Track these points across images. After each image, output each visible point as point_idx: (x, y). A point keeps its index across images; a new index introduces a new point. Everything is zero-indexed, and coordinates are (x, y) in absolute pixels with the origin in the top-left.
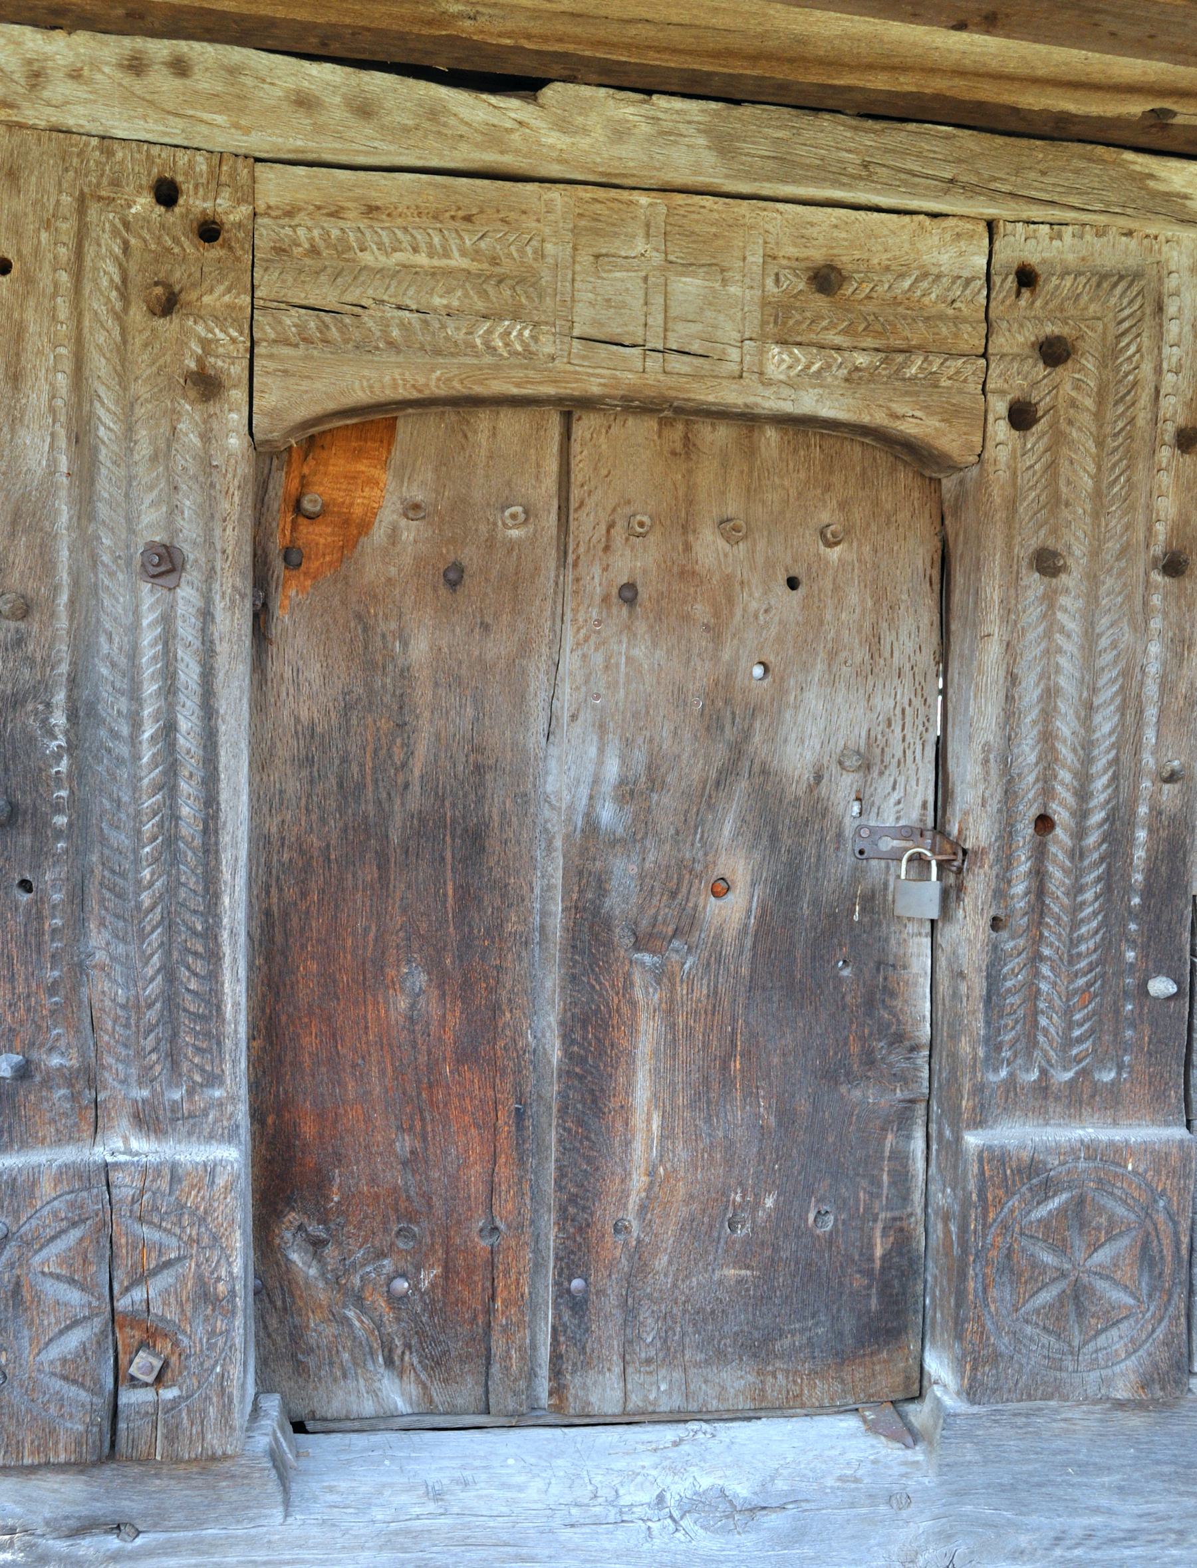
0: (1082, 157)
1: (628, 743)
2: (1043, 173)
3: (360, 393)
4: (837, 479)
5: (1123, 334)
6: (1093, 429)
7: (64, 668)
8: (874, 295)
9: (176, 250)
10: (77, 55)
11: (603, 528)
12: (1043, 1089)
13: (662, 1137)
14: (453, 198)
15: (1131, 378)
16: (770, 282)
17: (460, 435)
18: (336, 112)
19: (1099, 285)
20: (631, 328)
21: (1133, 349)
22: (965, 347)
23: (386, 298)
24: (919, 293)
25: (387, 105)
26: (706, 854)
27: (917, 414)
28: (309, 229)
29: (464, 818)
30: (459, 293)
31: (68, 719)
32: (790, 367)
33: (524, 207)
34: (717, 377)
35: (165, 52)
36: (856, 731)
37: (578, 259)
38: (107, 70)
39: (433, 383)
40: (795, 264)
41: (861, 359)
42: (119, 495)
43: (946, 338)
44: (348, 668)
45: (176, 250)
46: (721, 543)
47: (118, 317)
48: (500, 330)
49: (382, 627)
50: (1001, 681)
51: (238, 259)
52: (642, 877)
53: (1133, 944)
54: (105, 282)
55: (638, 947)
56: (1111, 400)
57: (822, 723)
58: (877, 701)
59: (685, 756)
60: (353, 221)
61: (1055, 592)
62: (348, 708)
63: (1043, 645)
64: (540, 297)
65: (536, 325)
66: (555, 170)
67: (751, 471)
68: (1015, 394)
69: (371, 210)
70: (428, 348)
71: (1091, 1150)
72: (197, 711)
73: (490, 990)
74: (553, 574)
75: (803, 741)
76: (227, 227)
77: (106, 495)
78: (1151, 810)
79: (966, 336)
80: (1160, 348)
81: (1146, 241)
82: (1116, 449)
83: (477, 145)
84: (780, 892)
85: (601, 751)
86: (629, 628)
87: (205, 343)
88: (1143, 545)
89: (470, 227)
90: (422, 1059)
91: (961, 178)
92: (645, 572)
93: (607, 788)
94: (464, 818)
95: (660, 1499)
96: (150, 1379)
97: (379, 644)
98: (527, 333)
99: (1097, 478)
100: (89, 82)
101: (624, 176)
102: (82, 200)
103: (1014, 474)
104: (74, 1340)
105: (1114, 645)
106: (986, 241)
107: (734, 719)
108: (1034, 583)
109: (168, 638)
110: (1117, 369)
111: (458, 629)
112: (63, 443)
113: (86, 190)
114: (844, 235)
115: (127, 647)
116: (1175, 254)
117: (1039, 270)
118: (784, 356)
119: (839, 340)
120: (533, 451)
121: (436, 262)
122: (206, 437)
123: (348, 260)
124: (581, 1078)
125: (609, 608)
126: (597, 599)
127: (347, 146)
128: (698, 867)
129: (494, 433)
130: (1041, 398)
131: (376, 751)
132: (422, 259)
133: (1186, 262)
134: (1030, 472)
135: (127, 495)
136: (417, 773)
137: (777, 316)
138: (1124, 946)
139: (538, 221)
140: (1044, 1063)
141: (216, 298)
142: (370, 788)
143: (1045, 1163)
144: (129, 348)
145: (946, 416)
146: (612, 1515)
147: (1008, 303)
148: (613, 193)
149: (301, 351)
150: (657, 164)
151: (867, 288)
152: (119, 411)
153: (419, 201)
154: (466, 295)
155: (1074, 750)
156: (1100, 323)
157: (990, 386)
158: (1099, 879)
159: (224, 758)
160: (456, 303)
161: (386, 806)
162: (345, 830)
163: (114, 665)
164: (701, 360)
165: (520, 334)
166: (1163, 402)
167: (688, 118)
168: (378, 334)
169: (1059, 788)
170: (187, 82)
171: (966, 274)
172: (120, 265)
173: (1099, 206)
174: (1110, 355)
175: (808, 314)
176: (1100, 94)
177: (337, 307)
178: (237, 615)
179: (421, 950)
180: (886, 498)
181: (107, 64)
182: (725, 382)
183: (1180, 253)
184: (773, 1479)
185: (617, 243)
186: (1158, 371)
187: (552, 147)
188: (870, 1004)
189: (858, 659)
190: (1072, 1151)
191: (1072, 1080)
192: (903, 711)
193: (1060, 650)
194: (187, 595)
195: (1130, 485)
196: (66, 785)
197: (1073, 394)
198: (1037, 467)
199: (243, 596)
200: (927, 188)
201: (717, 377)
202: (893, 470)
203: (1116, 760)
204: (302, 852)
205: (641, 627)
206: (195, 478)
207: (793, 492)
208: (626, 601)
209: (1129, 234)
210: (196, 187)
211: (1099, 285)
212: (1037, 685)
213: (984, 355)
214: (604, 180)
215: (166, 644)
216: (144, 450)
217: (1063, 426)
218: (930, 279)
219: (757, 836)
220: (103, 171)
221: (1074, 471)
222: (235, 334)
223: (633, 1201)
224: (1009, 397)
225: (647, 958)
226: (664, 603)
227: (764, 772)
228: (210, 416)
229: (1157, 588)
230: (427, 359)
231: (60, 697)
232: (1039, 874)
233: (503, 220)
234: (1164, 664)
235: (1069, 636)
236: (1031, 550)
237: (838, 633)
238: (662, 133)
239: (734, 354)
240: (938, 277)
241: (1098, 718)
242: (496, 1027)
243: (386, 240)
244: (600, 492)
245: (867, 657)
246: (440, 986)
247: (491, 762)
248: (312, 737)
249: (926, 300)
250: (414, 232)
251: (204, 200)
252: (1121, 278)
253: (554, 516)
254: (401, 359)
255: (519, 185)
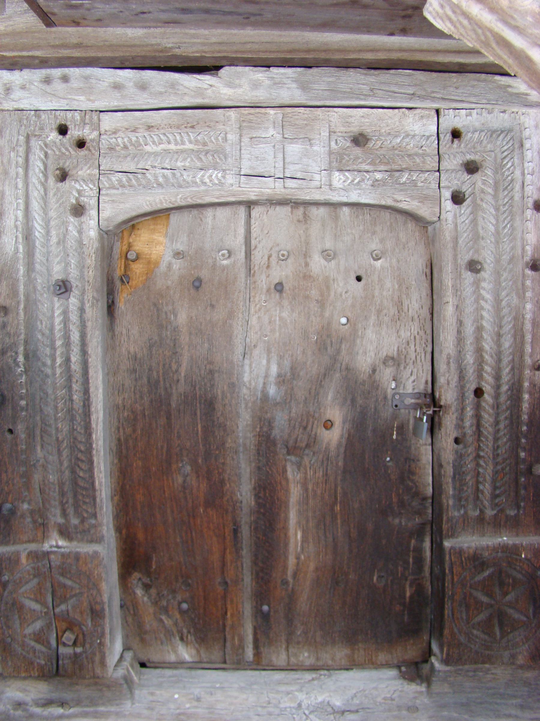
0: (475, 80)
1: (281, 357)
2: (457, 88)
3: (146, 207)
4: (378, 228)
5: (505, 158)
6: (493, 203)
7: (22, 337)
8: (383, 146)
9: (67, 153)
10: (24, 79)
11: (266, 258)
12: (481, 520)
13: (303, 542)
14: (185, 119)
15: (510, 178)
16: (333, 143)
17: (199, 220)
18: (131, 89)
19: (491, 136)
20: (268, 169)
21: (510, 164)
22: (428, 167)
23: (156, 165)
24: (404, 144)
25: (153, 84)
26: (320, 409)
27: (407, 199)
28: (123, 138)
29: (205, 395)
30: (189, 160)
31: (25, 359)
32: (344, 182)
33: (217, 120)
34: (309, 188)
35: (59, 74)
36: (392, 347)
37: (243, 140)
38: (36, 84)
39: (179, 200)
40: (345, 135)
41: (378, 176)
42: (44, 260)
43: (419, 164)
44: (151, 328)
45: (67, 153)
46: (323, 262)
47: (43, 184)
48: (208, 174)
49: (165, 309)
50: (454, 324)
51: (93, 154)
52: (290, 420)
53: (524, 449)
54: (37, 170)
55: (288, 453)
56: (501, 188)
57: (375, 344)
58: (402, 333)
59: (308, 363)
60: (142, 133)
61: (479, 280)
62: (151, 347)
63: (475, 306)
64: (226, 158)
65: (224, 171)
66: (230, 104)
67: (336, 227)
68: (455, 188)
69: (149, 128)
70: (176, 185)
71: (504, 548)
72: (79, 352)
73: (220, 474)
74: (243, 280)
75: (366, 353)
76: (88, 141)
77: (39, 261)
78: (530, 384)
79: (428, 162)
80: (523, 163)
81: (512, 115)
82: (505, 212)
83: (192, 97)
84: (357, 426)
85: (268, 362)
86: (280, 303)
87: (79, 192)
88: (521, 257)
89: (193, 130)
90: (190, 505)
91: (417, 93)
92: (287, 277)
93: (272, 379)
94: (205, 395)
95: (300, 705)
96: (71, 643)
97: (164, 316)
98: (220, 175)
99: (496, 226)
100: (29, 90)
101: (261, 103)
102: (28, 138)
103: (456, 226)
104: (38, 625)
105: (509, 305)
106: (436, 119)
107: (332, 344)
108: (469, 277)
109: (66, 321)
110: (503, 174)
111: (200, 308)
112: (20, 240)
113: (29, 133)
114: (367, 120)
115: (49, 326)
116: (527, 120)
117: (462, 130)
118: (341, 177)
119: (367, 168)
120: (232, 225)
121: (179, 147)
122: (80, 232)
123: (140, 150)
124: (264, 514)
125: (270, 294)
126: (264, 291)
127: (136, 102)
128: (317, 415)
129: (214, 217)
130: (466, 189)
131: (164, 365)
132: (172, 147)
133: (532, 123)
134: (464, 224)
135: (47, 260)
136: (183, 375)
137: (337, 159)
138: (519, 450)
139: (224, 125)
140: (482, 507)
141: (84, 172)
142: (162, 383)
143: (481, 555)
144: (48, 196)
145: (421, 200)
146: (277, 711)
147: (448, 146)
148: (258, 110)
149: (120, 191)
150: (274, 97)
151: (379, 143)
152: (43, 224)
153: (170, 122)
154: (192, 160)
155: (492, 356)
156: (493, 153)
157: (442, 185)
158: (506, 418)
159: (91, 372)
160: (187, 164)
161: (169, 390)
162: (151, 402)
163: (43, 334)
164: (302, 181)
165: (217, 176)
166: (526, 189)
167: (287, 76)
168: (153, 181)
169: (485, 374)
170: (69, 85)
171: (427, 134)
172: (44, 163)
173: (484, 101)
174: (499, 168)
175: (352, 157)
176: (471, 55)
177: (136, 171)
178: (95, 309)
179: (187, 455)
180: (402, 236)
181: (36, 81)
182: (313, 190)
183: (530, 119)
184: (352, 699)
185: (260, 131)
186: (523, 174)
187: (225, 94)
188: (402, 479)
189: (392, 313)
190: (495, 549)
191: (495, 515)
192: (415, 337)
193: (482, 308)
194: (73, 301)
195: (513, 228)
196: (24, 387)
197: (483, 186)
198: (467, 222)
199: (97, 301)
200: (402, 98)
201: (309, 188)
202: (405, 223)
203: (513, 360)
204: (133, 412)
205: (286, 303)
206: (76, 250)
207: (357, 236)
208: (278, 291)
209: (504, 112)
210: (75, 126)
211: (491, 136)
212: (473, 325)
213: (438, 171)
214: (252, 105)
215: (65, 324)
216: (54, 240)
217: (479, 201)
218: (410, 137)
219: (345, 399)
220: (36, 124)
221: (485, 223)
222: (92, 186)
223: (290, 572)
224: (451, 190)
225: (293, 458)
226: (296, 291)
227: (347, 369)
228: (82, 223)
229: (528, 277)
230: (175, 190)
231: (21, 349)
232: (478, 417)
233: (208, 126)
234: (534, 313)
235: (486, 302)
236: (466, 261)
237: (382, 301)
238: (275, 84)
239: (317, 177)
240: (414, 136)
241: (502, 340)
242: (223, 491)
243: (156, 140)
244: (264, 241)
245: (396, 312)
246: (197, 472)
247: (217, 369)
248: (136, 360)
249: (408, 147)
250: (168, 135)
251: (79, 131)
252: (502, 132)
253: (243, 254)
254: (164, 191)
255: (215, 110)
